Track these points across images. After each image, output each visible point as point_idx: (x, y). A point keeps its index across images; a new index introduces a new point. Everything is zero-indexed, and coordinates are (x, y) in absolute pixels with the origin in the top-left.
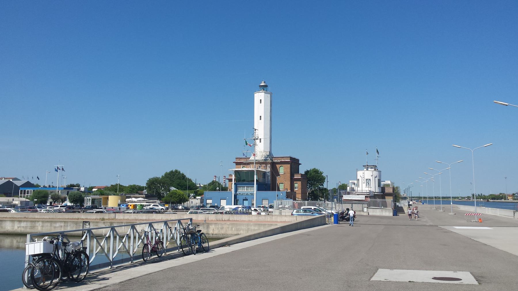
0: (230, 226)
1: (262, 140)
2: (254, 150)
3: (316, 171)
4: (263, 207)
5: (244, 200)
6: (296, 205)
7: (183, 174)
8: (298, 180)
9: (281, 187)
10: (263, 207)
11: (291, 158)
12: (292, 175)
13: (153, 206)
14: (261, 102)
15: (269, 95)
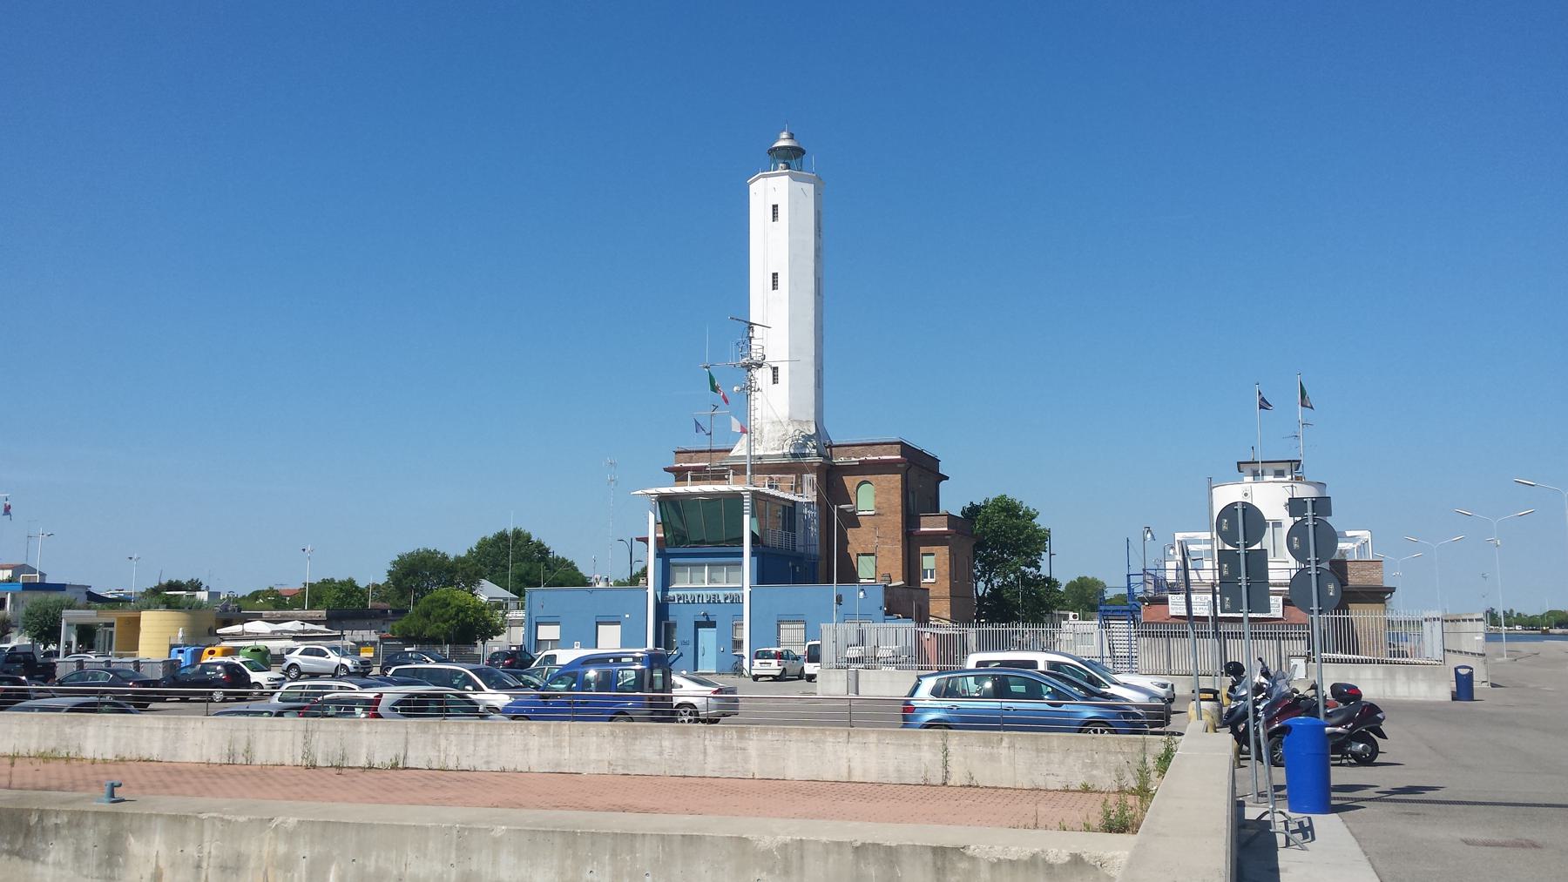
0: (304, 850)
1: (783, 374)
2: (744, 412)
3: (1008, 509)
4: (779, 656)
5: (698, 625)
6: (931, 647)
7: (540, 545)
8: (935, 539)
9: (865, 569)
10: (779, 656)
11: (906, 449)
12: (910, 521)
13: (305, 652)
14: (775, 216)
15: (809, 188)
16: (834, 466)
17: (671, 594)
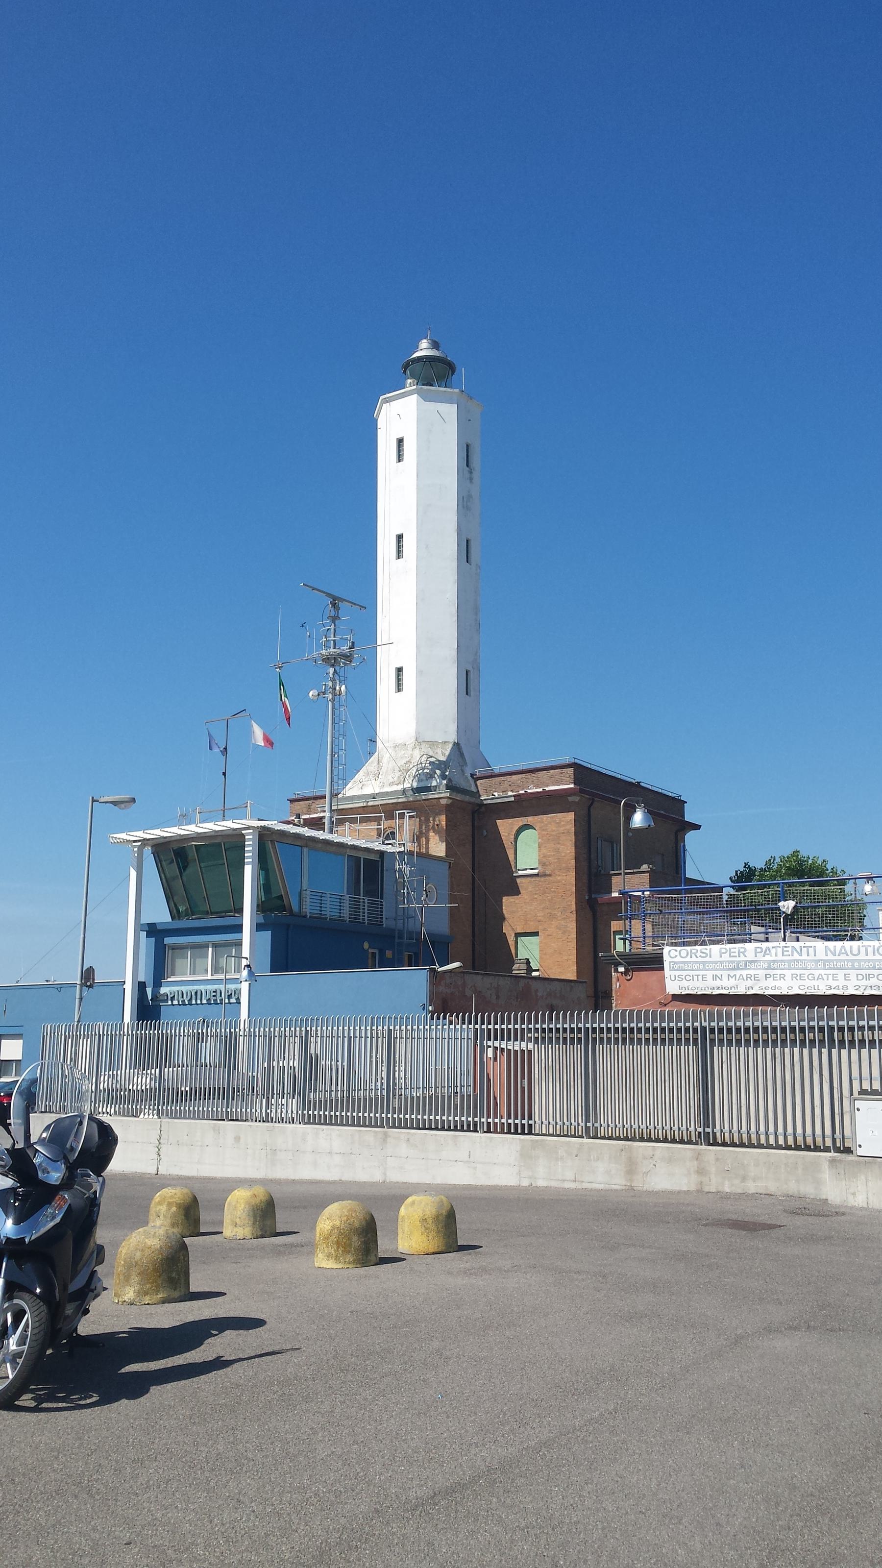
11: (575, 766)
15: (450, 411)
16: (481, 805)
17: (163, 990)
